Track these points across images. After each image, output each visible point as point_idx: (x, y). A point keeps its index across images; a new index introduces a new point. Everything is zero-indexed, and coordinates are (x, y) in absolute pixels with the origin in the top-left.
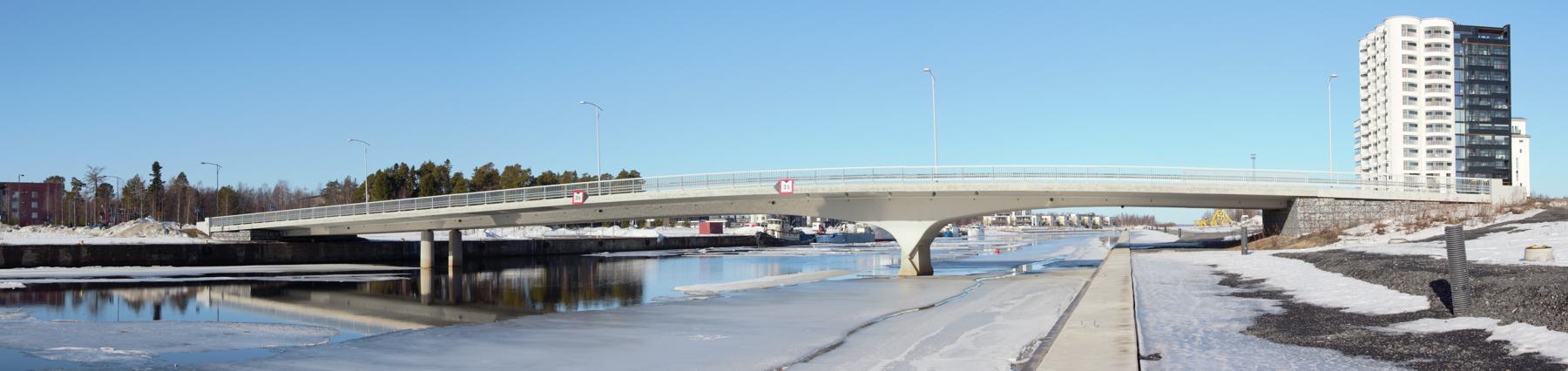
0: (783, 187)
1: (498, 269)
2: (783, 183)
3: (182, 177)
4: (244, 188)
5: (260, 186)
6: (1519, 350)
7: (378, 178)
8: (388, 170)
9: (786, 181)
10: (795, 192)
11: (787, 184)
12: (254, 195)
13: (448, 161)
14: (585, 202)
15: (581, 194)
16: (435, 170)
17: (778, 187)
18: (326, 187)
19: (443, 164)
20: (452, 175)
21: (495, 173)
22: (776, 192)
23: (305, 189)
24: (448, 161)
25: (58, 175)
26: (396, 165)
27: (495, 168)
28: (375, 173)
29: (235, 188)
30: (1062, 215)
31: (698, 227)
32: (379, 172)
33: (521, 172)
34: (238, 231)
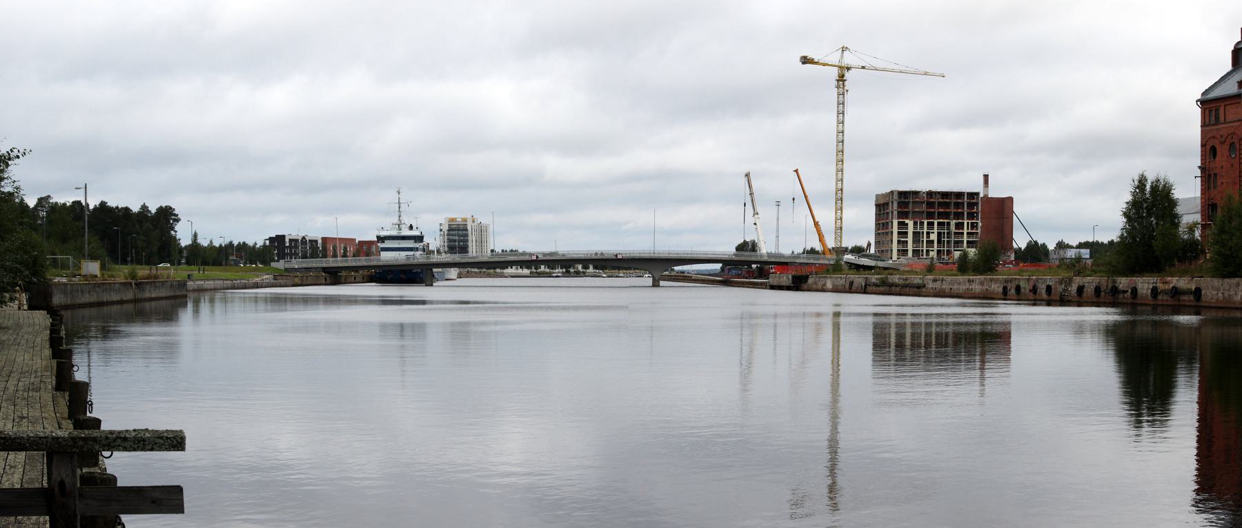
14: (538, 259)
17: (616, 256)
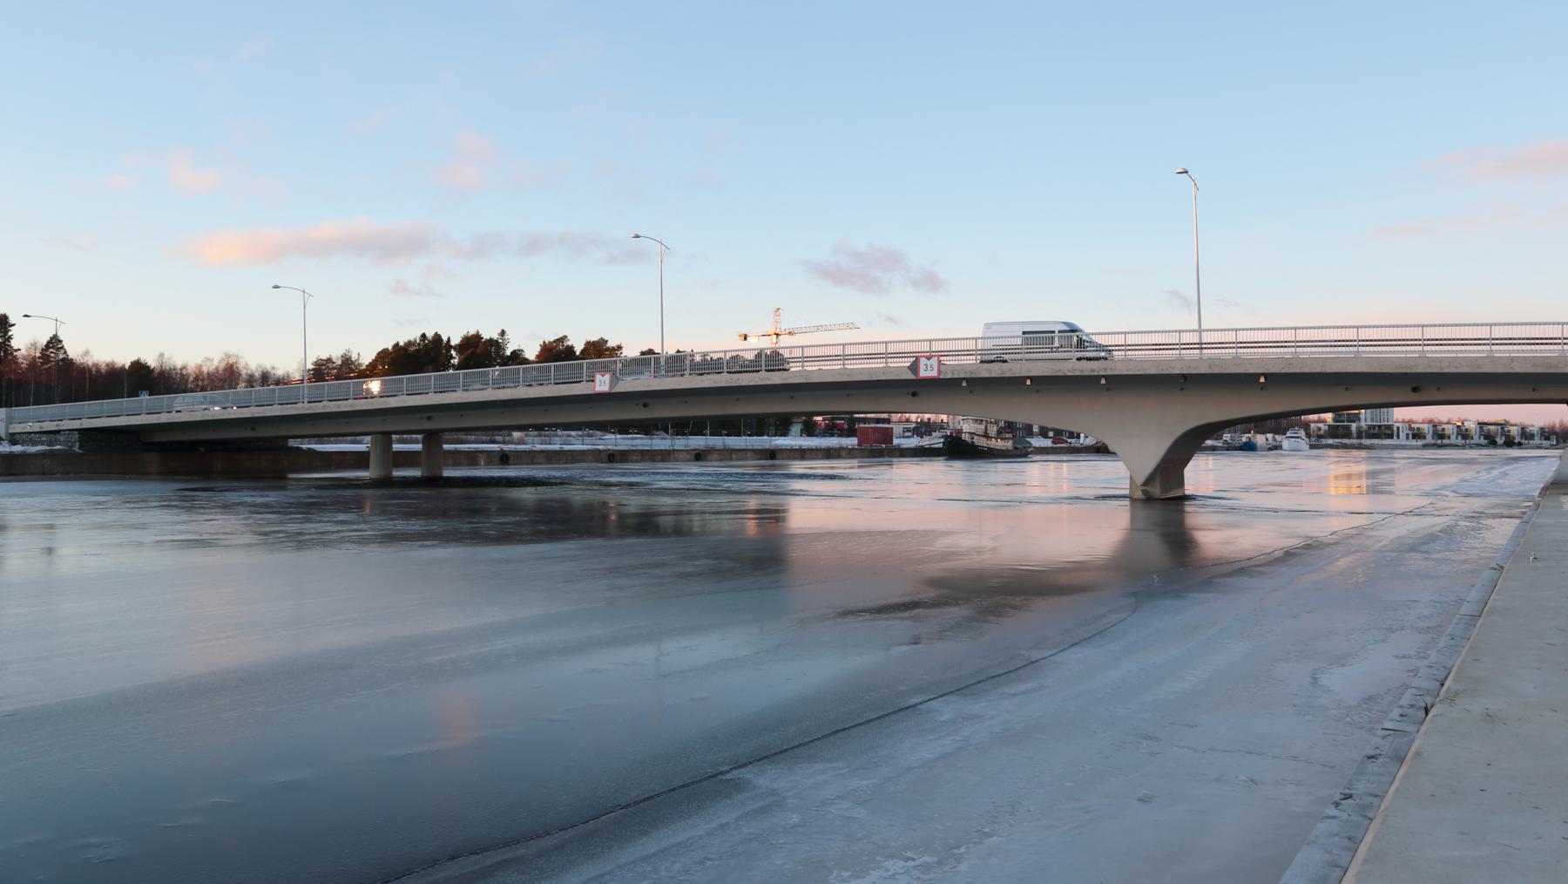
0: (922, 367)
1: (1300, 416)
2: (923, 361)
3: (55, 342)
4: (167, 366)
5: (199, 361)
6: (1363, 467)
7: (393, 355)
8: (409, 344)
9: (929, 358)
10: (942, 377)
11: (929, 363)
12: (188, 375)
13: (503, 333)
15: (607, 377)
16: (481, 345)
17: (914, 367)
18: (313, 367)
19: (495, 337)
20: (508, 353)
21: (570, 349)
22: (911, 377)
23: (274, 368)
24: (503, 333)
25: (268, 365)
26: (424, 336)
27: (570, 343)
28: (390, 348)
29: (152, 361)
30: (1448, 423)
31: (1395, 420)
32: (397, 345)
33: (608, 349)
34: (58, 432)
